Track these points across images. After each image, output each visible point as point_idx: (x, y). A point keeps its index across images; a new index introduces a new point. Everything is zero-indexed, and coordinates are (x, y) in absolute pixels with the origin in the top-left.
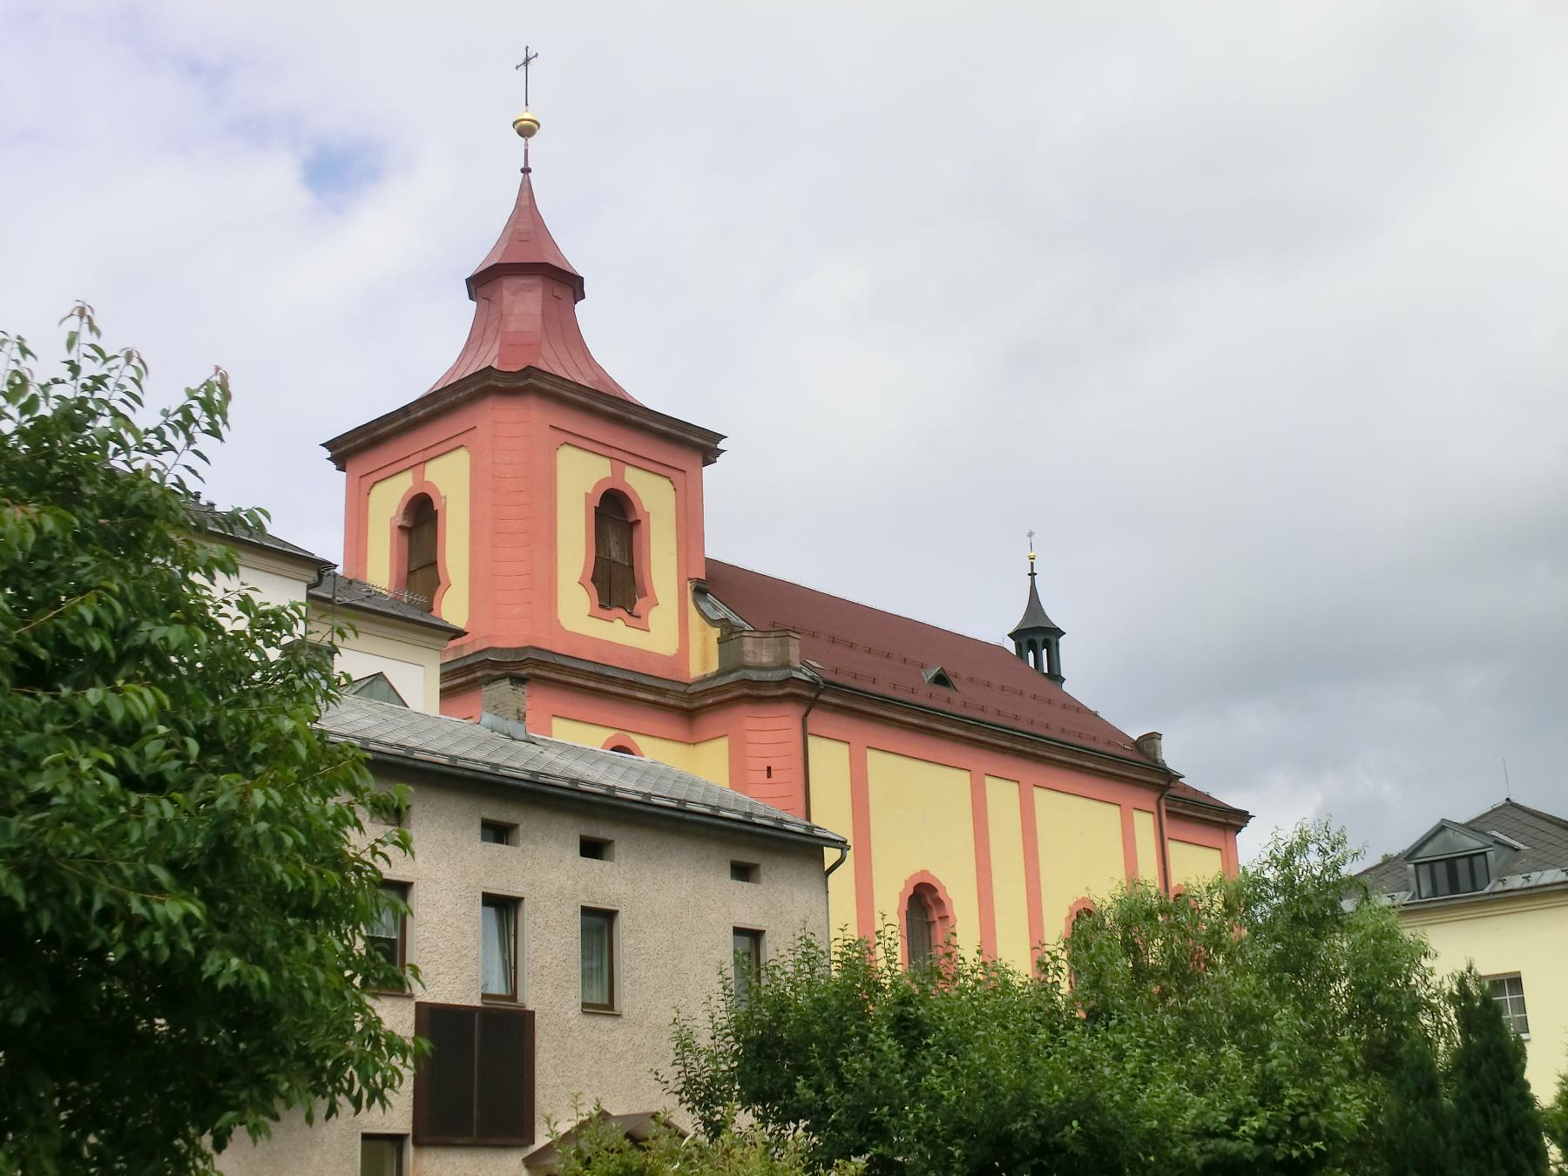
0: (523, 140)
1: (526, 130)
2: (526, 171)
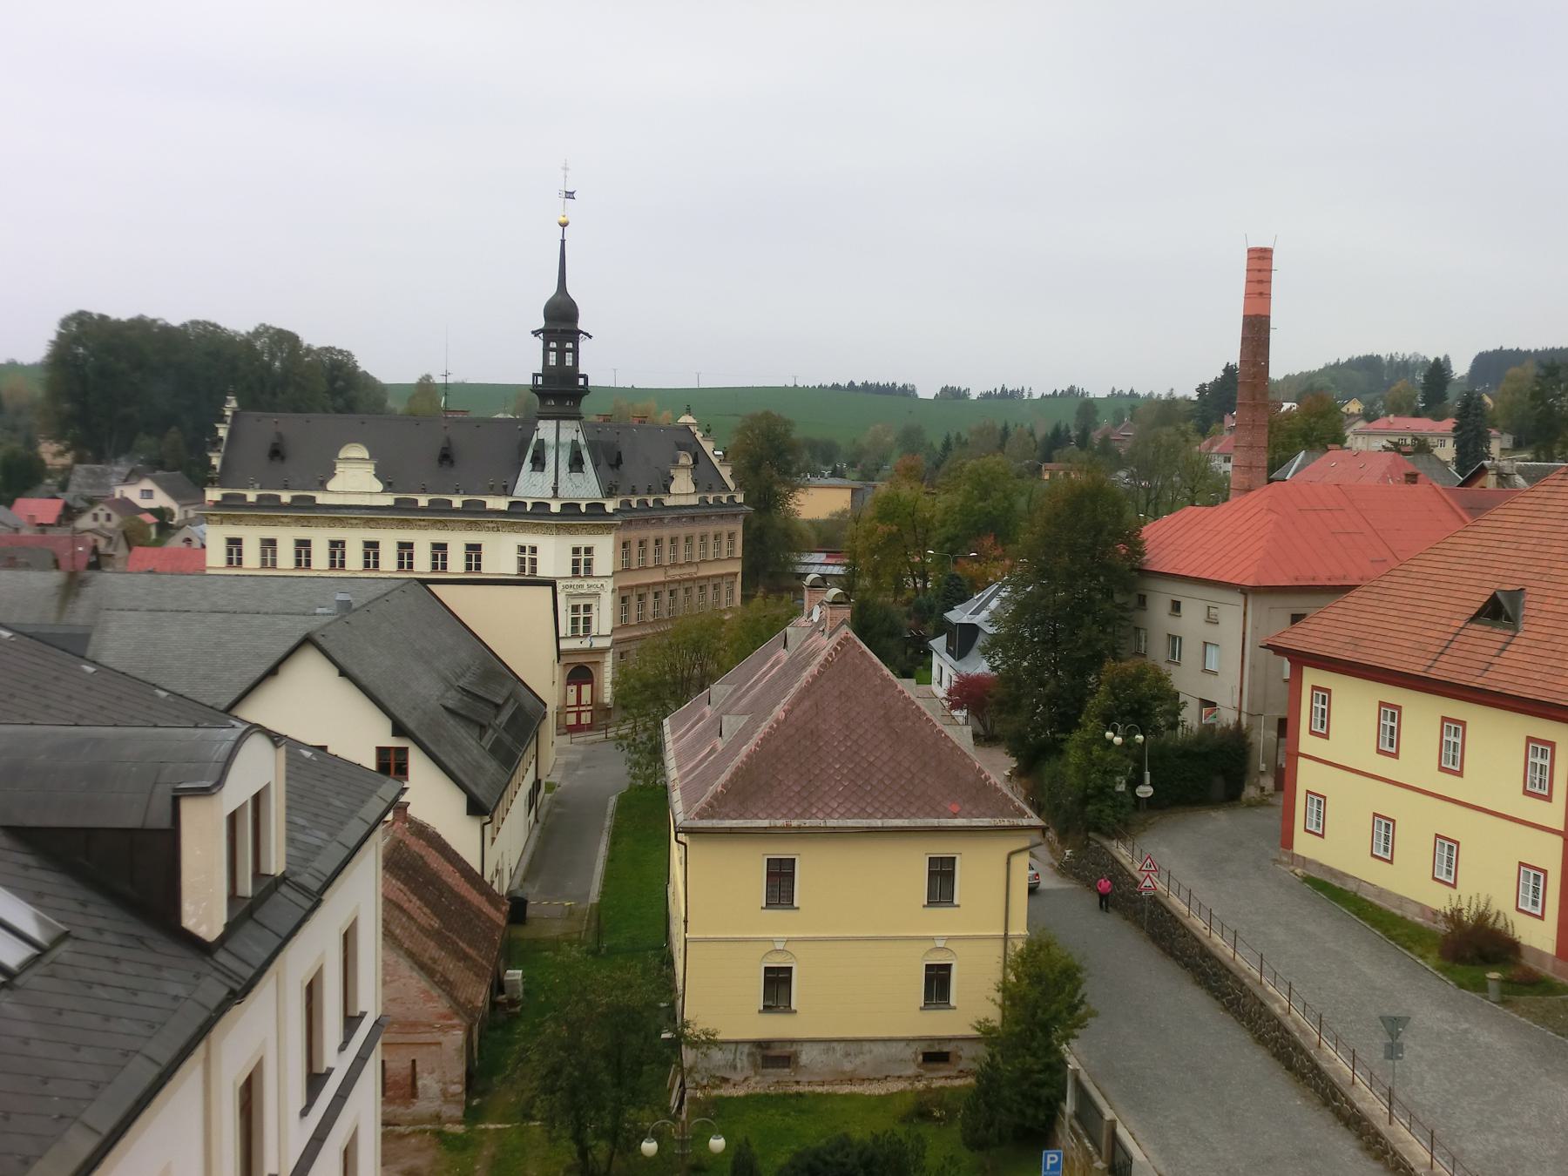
1: (564, 225)
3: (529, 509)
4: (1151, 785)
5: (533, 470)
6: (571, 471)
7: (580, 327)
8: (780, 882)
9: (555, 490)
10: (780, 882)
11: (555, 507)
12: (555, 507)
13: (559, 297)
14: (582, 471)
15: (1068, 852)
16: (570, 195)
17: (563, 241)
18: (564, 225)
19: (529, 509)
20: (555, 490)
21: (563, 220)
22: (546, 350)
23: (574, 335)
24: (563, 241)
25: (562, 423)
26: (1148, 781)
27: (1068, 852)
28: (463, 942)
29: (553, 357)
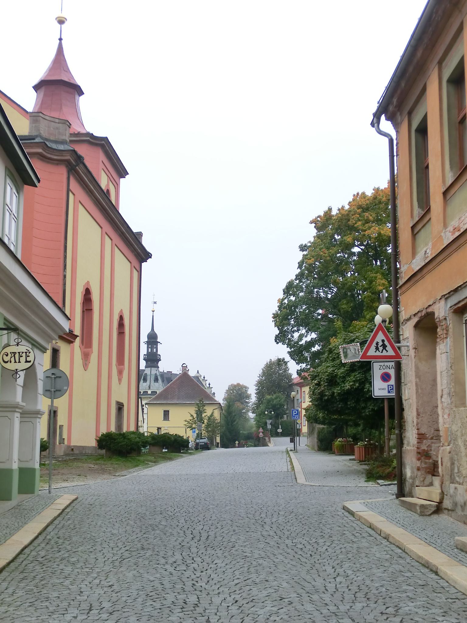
0: (59, 26)
1: (61, 22)
2: (60, 39)
3: (142, 394)
4: (281, 429)
5: (143, 382)
6: (155, 382)
7: (158, 341)
8: (166, 414)
9: (149, 387)
10: (166, 414)
11: (149, 392)
12: (149, 392)
13: (152, 332)
14: (158, 382)
15: (398, 275)
16: (155, 303)
17: (153, 316)
18: (153, 311)
19: (142, 394)
20: (149, 387)
21: (153, 310)
22: (148, 348)
23: (156, 343)
24: (153, 316)
25: (152, 368)
26: (280, 428)
27: (398, 275)
28: (411, 449)
29: (150, 349)
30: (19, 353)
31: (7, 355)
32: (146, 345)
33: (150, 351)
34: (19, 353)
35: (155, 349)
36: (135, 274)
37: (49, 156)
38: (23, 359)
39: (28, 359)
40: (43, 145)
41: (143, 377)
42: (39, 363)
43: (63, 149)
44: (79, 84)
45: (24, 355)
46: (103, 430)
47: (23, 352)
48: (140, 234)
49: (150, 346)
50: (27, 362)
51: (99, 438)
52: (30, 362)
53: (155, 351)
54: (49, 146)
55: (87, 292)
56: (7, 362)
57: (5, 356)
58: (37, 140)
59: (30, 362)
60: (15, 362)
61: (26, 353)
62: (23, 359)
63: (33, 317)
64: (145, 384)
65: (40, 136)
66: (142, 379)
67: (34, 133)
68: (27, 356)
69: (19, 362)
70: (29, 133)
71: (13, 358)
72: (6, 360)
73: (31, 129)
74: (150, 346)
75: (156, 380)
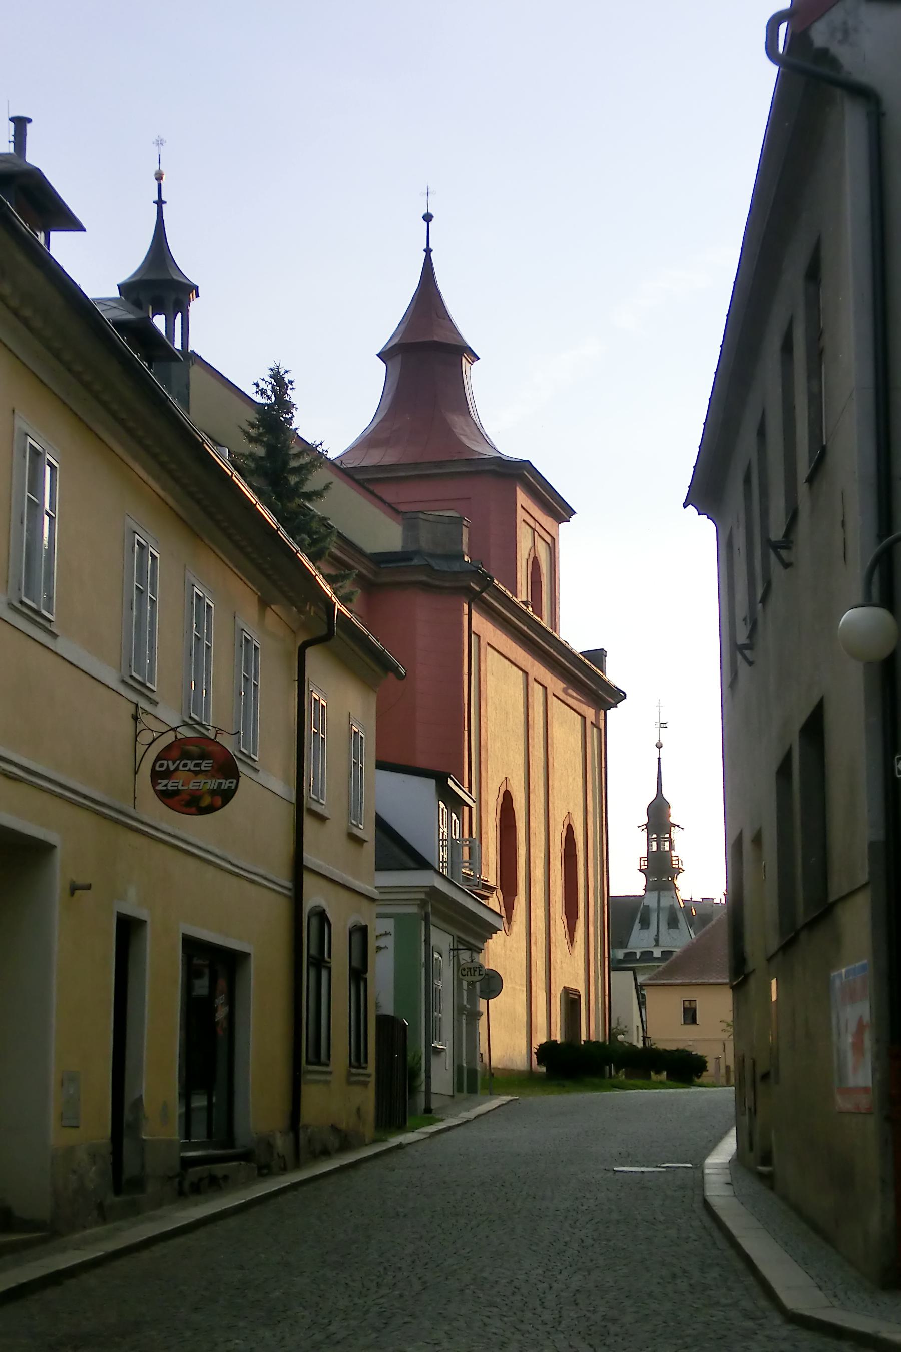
9: (657, 941)
11: (657, 953)
12: (657, 953)
17: (659, 758)
20: (657, 941)
24: (659, 758)
29: (654, 844)
30: (474, 968)
31: (464, 970)
32: (645, 834)
33: (654, 848)
34: (474, 968)
35: (667, 844)
36: (592, 733)
37: (437, 583)
38: (477, 973)
39: (481, 973)
40: (428, 569)
41: (639, 916)
42: (463, 959)
43: (459, 570)
44: (470, 345)
45: (477, 970)
46: (540, 1038)
47: (476, 968)
48: (598, 656)
49: (655, 836)
50: (480, 975)
51: (539, 1046)
52: (482, 975)
53: (667, 849)
54: (436, 568)
55: (507, 798)
56: (465, 976)
57: (462, 971)
58: (416, 562)
59: (482, 975)
60: (471, 975)
61: (479, 968)
62: (477, 973)
63: (475, 928)
64: (645, 933)
65: (418, 553)
66: (637, 921)
67: (412, 547)
68: (480, 971)
69: (474, 975)
70: (403, 547)
71: (469, 973)
72: (464, 974)
73: (405, 540)
74: (655, 836)
75: (673, 923)
